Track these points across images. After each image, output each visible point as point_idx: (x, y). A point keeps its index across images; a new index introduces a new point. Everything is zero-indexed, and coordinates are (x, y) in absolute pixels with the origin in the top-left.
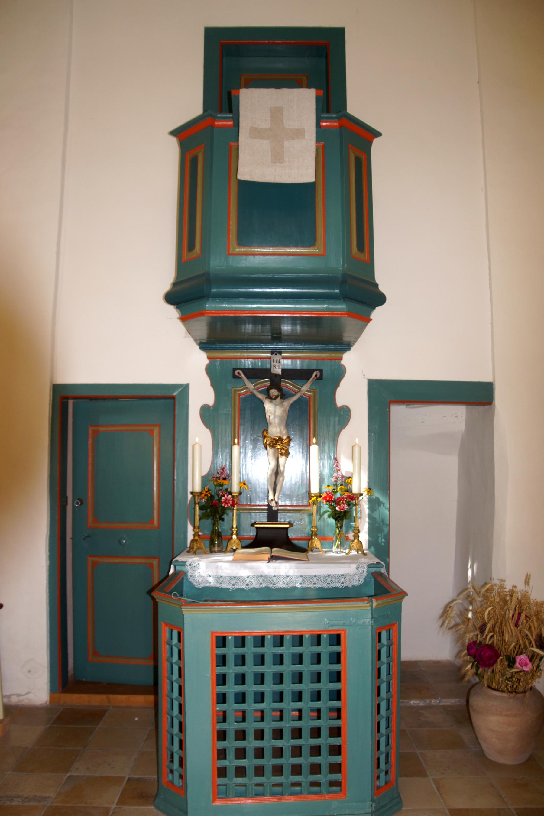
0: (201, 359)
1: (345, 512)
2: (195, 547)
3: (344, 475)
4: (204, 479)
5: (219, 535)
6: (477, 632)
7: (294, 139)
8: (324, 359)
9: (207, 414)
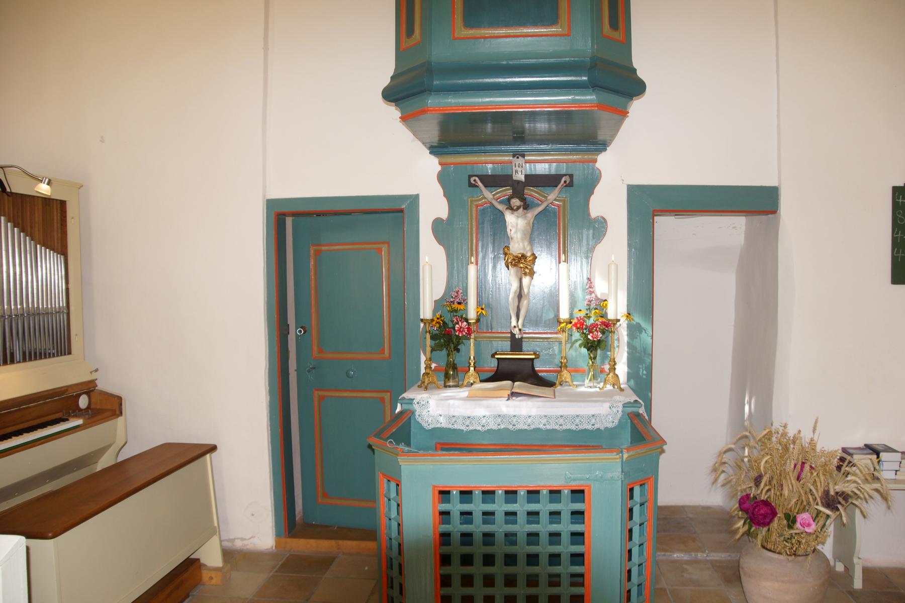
0: (432, 165)
1: (599, 341)
2: (426, 382)
3: (599, 296)
4: (438, 304)
5: (455, 367)
6: (752, 484)
8: (574, 161)
9: (440, 229)
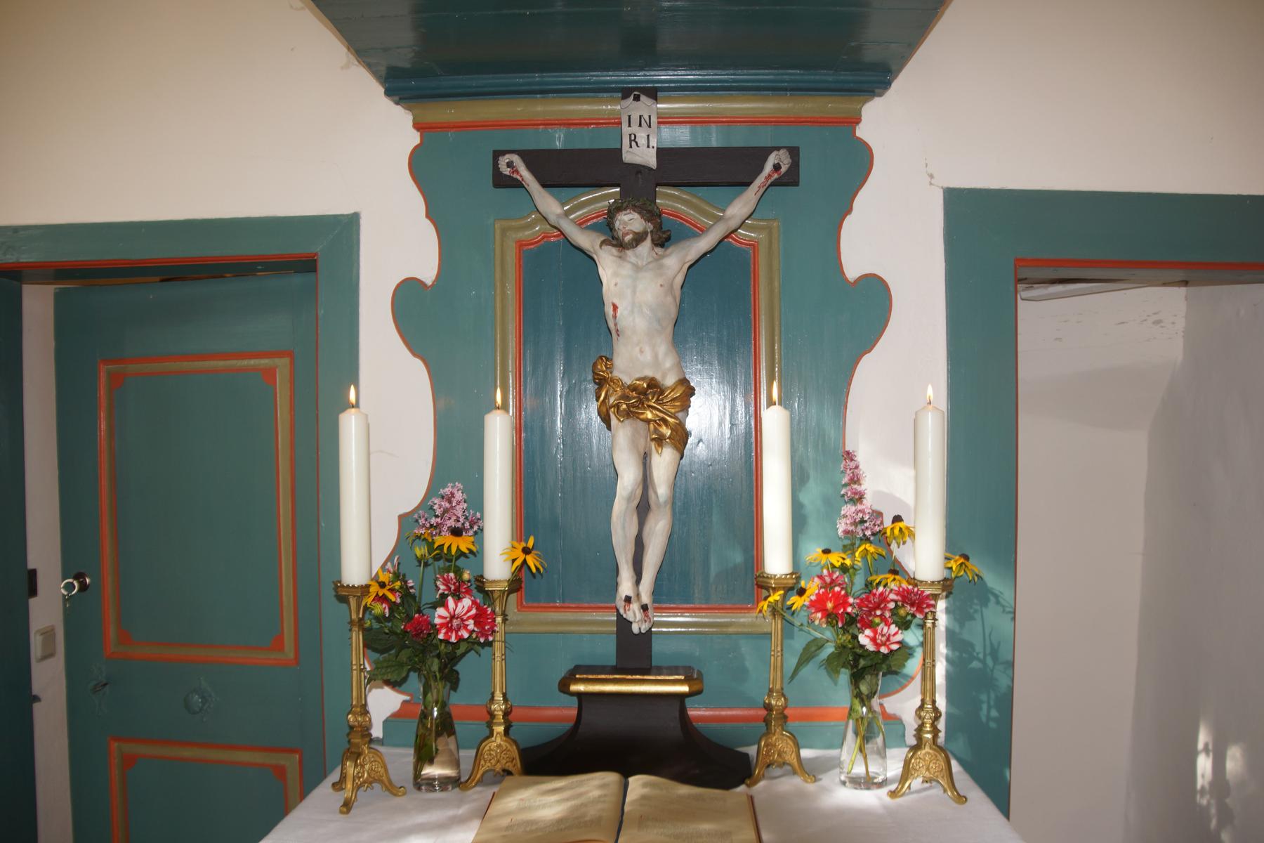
0: (393, 130)
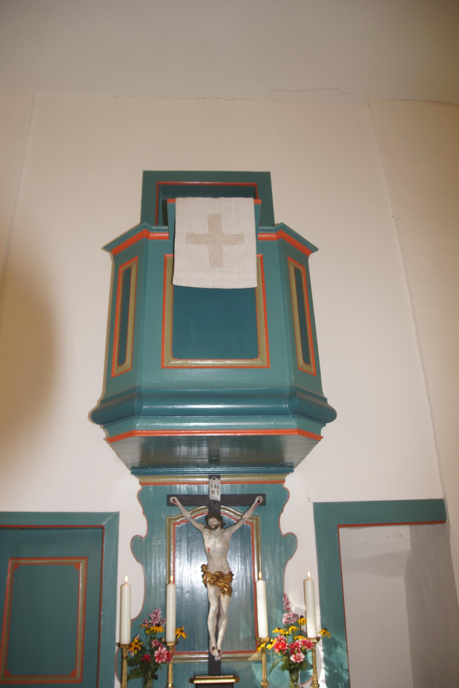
0: (133, 484)
7: (233, 245)
8: (265, 482)
